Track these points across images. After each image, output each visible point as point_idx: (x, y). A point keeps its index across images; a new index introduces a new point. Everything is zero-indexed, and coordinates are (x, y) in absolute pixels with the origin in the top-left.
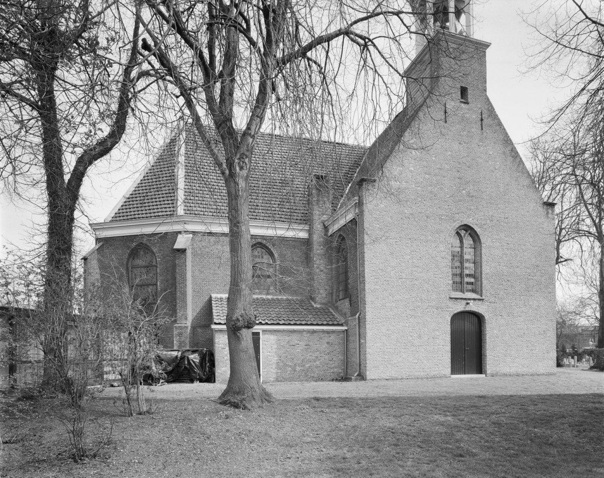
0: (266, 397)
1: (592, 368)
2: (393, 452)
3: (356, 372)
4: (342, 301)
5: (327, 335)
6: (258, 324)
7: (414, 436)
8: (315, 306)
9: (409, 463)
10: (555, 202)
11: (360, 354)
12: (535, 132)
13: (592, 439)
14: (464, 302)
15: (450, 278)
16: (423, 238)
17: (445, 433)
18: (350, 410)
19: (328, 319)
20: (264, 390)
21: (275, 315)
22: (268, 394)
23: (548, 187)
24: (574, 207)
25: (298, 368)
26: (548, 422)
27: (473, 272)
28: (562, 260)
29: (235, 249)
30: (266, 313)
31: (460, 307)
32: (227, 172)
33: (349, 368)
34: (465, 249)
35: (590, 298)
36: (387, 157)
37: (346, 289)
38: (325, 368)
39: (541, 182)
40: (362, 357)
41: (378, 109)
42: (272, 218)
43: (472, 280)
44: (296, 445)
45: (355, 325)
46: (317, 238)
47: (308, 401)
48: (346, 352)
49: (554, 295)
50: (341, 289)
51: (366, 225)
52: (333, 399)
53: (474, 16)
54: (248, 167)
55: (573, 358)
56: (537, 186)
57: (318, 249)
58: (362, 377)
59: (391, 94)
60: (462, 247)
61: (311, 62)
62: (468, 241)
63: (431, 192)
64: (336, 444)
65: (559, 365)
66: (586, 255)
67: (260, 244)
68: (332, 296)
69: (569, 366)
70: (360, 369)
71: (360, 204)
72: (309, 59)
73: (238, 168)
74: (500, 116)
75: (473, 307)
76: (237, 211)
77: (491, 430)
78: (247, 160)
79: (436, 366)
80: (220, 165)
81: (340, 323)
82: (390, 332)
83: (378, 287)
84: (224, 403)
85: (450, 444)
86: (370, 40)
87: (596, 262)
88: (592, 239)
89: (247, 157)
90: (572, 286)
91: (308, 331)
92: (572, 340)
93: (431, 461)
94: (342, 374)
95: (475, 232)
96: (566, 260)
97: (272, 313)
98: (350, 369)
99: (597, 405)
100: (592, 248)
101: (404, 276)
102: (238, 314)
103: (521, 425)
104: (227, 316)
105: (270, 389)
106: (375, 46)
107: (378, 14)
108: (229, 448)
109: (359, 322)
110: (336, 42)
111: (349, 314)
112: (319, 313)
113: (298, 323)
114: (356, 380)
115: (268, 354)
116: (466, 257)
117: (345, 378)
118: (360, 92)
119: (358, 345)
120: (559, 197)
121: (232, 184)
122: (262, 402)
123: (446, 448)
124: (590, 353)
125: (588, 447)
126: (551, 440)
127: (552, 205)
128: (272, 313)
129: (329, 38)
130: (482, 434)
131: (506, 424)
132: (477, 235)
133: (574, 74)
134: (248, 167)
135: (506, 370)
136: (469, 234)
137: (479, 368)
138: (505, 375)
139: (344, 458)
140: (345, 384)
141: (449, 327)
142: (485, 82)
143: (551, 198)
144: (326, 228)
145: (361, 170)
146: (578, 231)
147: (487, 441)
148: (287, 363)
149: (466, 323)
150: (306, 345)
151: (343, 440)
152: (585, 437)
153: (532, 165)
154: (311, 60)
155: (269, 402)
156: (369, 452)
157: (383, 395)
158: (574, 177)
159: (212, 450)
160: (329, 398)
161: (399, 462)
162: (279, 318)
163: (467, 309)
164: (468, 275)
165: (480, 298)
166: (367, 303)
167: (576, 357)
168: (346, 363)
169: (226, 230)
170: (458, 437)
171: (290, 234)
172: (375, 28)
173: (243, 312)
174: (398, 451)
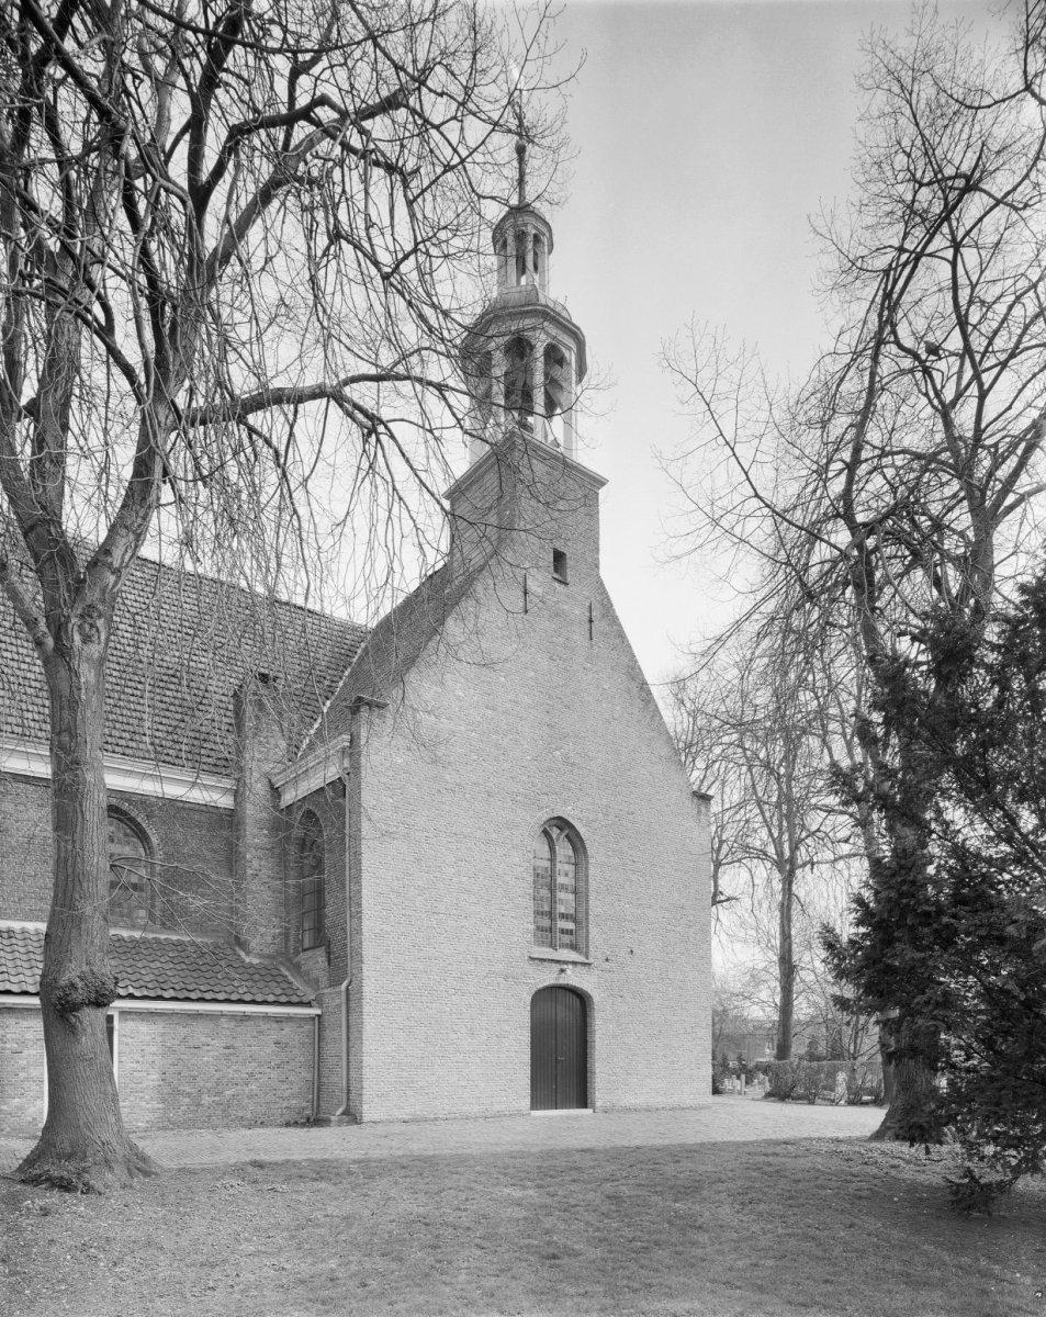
0: (140, 1166)
1: (769, 1095)
2: (430, 1260)
3: (339, 1106)
4: (310, 953)
5: (274, 1025)
6: (120, 997)
7: (469, 1228)
8: (247, 960)
9: (462, 1277)
10: (710, 793)
11: (348, 1068)
12: (685, 666)
13: (760, 1214)
14: (556, 967)
15: (531, 919)
16: (479, 834)
17: (525, 1219)
18: (335, 1184)
19: (278, 991)
20: (133, 1147)
21: (152, 977)
22: (144, 1159)
23: (701, 764)
24: (741, 805)
25: (206, 1100)
26: (697, 1189)
27: (572, 911)
28: (723, 898)
29: (66, 821)
30: (129, 970)
31: (548, 977)
32: (50, 642)
33: (324, 1096)
34: (559, 866)
35: (765, 969)
36: (411, 661)
37: (319, 929)
38: (270, 1098)
39: (690, 752)
40: (352, 1074)
41: (396, 566)
42: (162, 757)
43: (570, 926)
44: (225, 1261)
45: (339, 1006)
46: (255, 811)
47: (239, 1170)
48: (318, 1063)
49: (709, 963)
50: (306, 926)
51: (367, 798)
52: (295, 1164)
53: (579, 432)
54: (103, 637)
55: (738, 1078)
56: (683, 758)
57: (255, 836)
58: (352, 1116)
59: (426, 547)
60: (552, 860)
61: (254, 436)
62: (564, 850)
63: (496, 745)
64: (311, 1252)
65: (716, 1091)
66: (760, 893)
67: (121, 812)
68: (287, 940)
69: (732, 1092)
70: (348, 1099)
71: (352, 751)
72: (251, 430)
73: (77, 637)
74: (602, 516)
75: (572, 978)
76: (73, 736)
77: (604, 1209)
78: (100, 623)
79: (503, 1093)
80: (31, 623)
81: (305, 999)
82: (413, 1023)
83: (389, 929)
84: (35, 1181)
85: (536, 1239)
86: (382, 422)
87: (775, 906)
88: (769, 865)
89: (100, 616)
90: (738, 946)
91: (232, 1017)
92: (738, 1046)
93: (502, 1271)
94: (308, 1112)
95: (578, 834)
96: (728, 900)
97: (143, 972)
98: (325, 1100)
99: (770, 1159)
100: (769, 881)
101: (442, 908)
102: (71, 973)
103: (655, 1198)
104: (43, 976)
105: (147, 1146)
106: (392, 437)
107: (398, 378)
108: (63, 1280)
109: (348, 999)
110: (313, 407)
111: (324, 981)
112: (257, 977)
113: (208, 996)
114: (340, 1123)
115: (135, 1065)
116: (561, 880)
117: (316, 1121)
118: (360, 521)
119: (344, 1049)
120: (717, 783)
121: (63, 673)
122: (131, 1174)
123: (528, 1246)
124: (766, 1069)
125: (755, 1228)
126: (700, 1221)
127: (706, 798)
128: (143, 972)
129: (299, 398)
130: (590, 1218)
131: (630, 1197)
132: (582, 840)
133: (739, 582)
134: (103, 637)
135: (629, 1100)
136: (567, 836)
137: (583, 1099)
138: (628, 1110)
139: (332, 1280)
140: (315, 1132)
141: (528, 1015)
142: (597, 549)
143: (705, 784)
144: (276, 792)
145: (360, 675)
146: (746, 848)
147: (598, 1229)
148: (181, 1088)
149: (559, 1007)
150: (228, 1048)
151: (325, 1244)
152: (751, 1212)
153: (674, 719)
154: (259, 435)
155: (147, 1174)
156: (382, 1264)
157: (400, 1153)
158: (740, 750)
159: (18, 1288)
160: (288, 1161)
161: (444, 1278)
162: (161, 985)
163: (562, 981)
164: (563, 916)
165: (580, 958)
166: (365, 959)
167: (743, 1076)
168: (318, 1088)
169: (43, 769)
170: (548, 1226)
171: (197, 796)
172: (393, 402)
173: (85, 968)
174: (440, 1257)
